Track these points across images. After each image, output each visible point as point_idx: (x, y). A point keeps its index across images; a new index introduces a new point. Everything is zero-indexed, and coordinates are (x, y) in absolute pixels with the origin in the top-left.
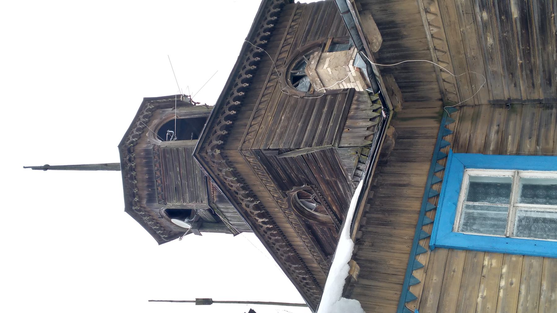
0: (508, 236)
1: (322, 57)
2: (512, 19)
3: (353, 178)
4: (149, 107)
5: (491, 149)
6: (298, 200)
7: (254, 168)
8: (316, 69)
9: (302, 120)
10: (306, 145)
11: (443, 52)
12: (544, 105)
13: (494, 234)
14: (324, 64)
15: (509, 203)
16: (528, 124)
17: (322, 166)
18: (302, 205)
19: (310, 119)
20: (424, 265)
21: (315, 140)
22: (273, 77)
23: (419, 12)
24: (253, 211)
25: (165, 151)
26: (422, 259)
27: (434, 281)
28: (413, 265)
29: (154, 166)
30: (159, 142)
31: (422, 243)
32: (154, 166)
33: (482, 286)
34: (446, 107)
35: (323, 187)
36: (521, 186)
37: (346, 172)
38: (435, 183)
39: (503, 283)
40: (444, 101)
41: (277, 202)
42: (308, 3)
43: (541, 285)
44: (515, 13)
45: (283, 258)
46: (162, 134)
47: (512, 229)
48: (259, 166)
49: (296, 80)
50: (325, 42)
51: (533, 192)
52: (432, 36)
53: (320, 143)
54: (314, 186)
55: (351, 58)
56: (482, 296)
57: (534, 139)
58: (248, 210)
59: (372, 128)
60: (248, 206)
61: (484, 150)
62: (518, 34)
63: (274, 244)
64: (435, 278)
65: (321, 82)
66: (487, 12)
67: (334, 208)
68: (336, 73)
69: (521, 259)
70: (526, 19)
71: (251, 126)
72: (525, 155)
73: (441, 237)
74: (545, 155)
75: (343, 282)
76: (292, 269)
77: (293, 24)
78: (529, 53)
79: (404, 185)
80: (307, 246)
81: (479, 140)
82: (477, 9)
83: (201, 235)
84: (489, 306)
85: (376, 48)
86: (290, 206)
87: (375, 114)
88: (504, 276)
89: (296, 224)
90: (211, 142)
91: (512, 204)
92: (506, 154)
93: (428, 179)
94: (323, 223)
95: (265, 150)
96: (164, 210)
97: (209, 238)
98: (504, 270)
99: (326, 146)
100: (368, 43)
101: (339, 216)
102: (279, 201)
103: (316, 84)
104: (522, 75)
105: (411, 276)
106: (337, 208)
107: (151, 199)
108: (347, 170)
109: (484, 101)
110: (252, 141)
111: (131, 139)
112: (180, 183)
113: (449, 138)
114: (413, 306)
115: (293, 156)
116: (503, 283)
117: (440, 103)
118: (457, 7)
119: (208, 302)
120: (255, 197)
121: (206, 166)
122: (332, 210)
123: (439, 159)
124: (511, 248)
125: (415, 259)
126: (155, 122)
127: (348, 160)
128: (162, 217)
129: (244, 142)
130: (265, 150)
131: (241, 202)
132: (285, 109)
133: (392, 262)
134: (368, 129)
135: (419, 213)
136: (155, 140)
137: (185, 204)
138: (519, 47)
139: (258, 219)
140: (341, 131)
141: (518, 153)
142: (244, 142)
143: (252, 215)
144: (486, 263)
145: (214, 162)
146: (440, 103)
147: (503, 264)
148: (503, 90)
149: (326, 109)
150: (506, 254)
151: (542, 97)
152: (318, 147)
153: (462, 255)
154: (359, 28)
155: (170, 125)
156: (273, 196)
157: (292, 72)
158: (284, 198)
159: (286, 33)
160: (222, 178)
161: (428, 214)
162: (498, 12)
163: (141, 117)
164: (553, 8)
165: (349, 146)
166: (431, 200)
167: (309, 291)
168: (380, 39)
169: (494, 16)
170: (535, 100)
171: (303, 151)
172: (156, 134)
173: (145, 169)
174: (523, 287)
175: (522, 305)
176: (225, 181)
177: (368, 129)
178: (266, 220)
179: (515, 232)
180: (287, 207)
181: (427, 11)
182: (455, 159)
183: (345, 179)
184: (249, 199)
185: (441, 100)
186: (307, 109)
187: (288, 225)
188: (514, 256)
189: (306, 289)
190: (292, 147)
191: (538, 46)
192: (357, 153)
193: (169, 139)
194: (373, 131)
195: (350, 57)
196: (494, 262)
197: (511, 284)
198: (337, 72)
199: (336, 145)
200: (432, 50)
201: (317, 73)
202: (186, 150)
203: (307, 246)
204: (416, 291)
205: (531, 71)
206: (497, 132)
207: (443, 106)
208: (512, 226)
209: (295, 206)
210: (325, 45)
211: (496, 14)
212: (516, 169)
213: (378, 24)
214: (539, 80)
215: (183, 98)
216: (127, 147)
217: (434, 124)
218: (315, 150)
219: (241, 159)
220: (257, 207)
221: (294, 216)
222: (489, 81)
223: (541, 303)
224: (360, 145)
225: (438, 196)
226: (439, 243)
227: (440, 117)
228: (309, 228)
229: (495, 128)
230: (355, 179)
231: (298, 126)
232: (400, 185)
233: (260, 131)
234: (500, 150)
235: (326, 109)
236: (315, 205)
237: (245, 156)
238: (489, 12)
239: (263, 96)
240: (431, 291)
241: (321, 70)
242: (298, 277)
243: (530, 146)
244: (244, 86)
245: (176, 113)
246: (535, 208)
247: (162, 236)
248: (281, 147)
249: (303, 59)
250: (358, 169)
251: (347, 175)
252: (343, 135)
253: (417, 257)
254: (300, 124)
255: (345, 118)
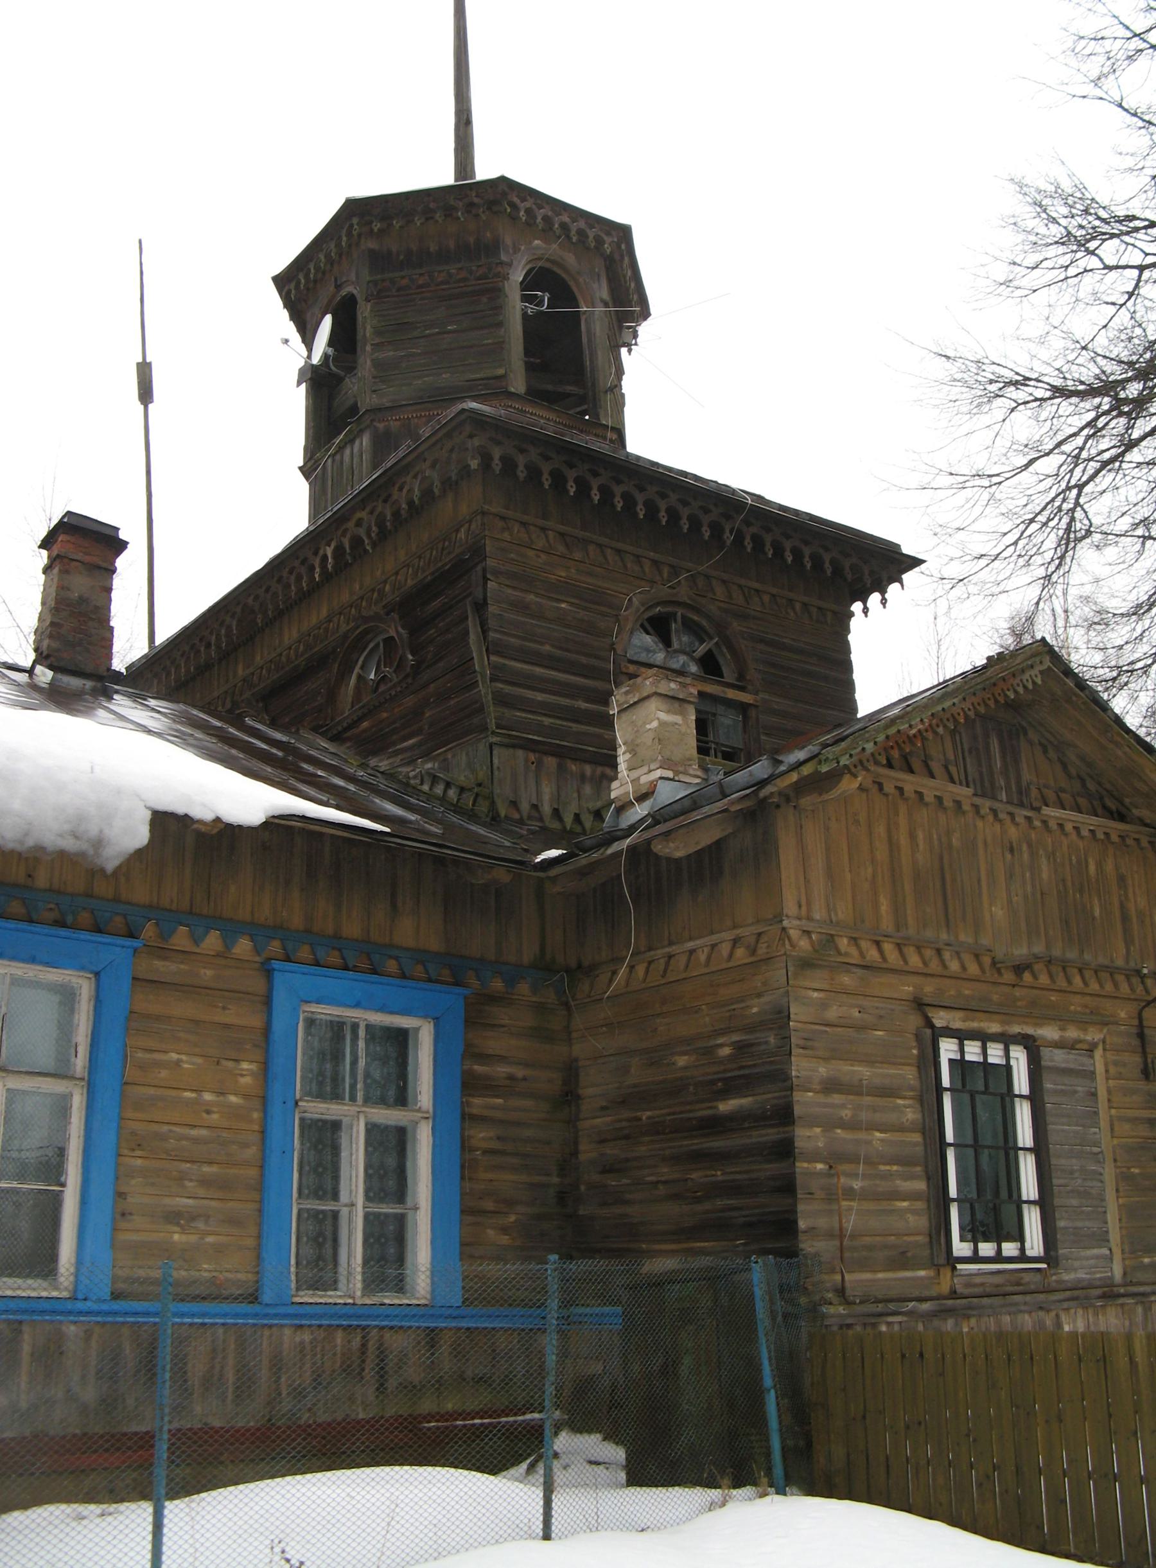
0: (300, 1104)
1: (686, 705)
2: (717, 1100)
3: (428, 773)
4: (608, 240)
5: (476, 1067)
6: (380, 638)
7: (444, 540)
8: (656, 694)
9: (558, 653)
10: (494, 667)
11: (665, 971)
12: (567, 1163)
13: (302, 1078)
14: (668, 712)
15: (367, 1100)
16: (528, 1133)
17: (452, 702)
18: (371, 645)
19: (559, 670)
20: (234, 951)
21: (508, 689)
22: (666, 571)
23: (735, 927)
24: (348, 536)
25: (494, 292)
26: (243, 947)
27: (202, 971)
28: (231, 928)
29: (459, 265)
30: (518, 275)
31: (275, 947)
32: (459, 265)
33: (199, 1060)
34: (565, 976)
35: (410, 701)
36: (401, 1124)
37: (442, 758)
38: (400, 964)
39: (208, 1097)
40: (580, 971)
41: (373, 590)
42: (850, 637)
43: (211, 1163)
44: (726, 1106)
45: (250, 601)
46: (541, 278)
47: (312, 1110)
48: (449, 553)
49: (659, 627)
50: (750, 687)
51: (391, 1147)
52: (692, 952)
53: (502, 700)
54: (410, 680)
55: (676, 773)
56: (182, 1061)
57: (495, 1145)
58: (351, 524)
59: (536, 815)
60: (359, 523)
61: (471, 1053)
62: (690, 1111)
63: (279, 581)
64: (209, 973)
65: (632, 705)
66: (730, 1055)
67: (365, 724)
68: (647, 739)
69: (256, 1127)
70: (716, 1125)
71: (543, 529)
72: (463, 1129)
73: (290, 982)
74: (463, 1167)
75: (181, 809)
76: (228, 619)
77: (798, 606)
78: (658, 1133)
79: (394, 905)
80: (281, 655)
81: (494, 1044)
82: (735, 1038)
83: (299, 384)
84: (164, 1073)
85: (658, 848)
86: (366, 619)
87: (568, 819)
88: (221, 1098)
89: (327, 630)
90: (499, 443)
91: (364, 1109)
92: (463, 1095)
93: (407, 949)
94: (332, 695)
95: (484, 570)
96: (355, 292)
97: (292, 407)
98: (233, 1099)
99: (492, 712)
100: (667, 834)
101: (348, 734)
102: (375, 595)
103: (627, 693)
104: (620, 1121)
105: (208, 929)
106: (364, 731)
107: (379, 261)
108: (445, 760)
109: (577, 1049)
110: (506, 536)
111: (522, 206)
112: (416, 333)
113: (498, 985)
114: (151, 934)
115: (472, 637)
116: (208, 1097)
117: (573, 964)
118: (741, 999)
119: (146, 394)
120: (384, 535)
121: (440, 434)
122: (360, 719)
123: (446, 968)
124: (276, 1110)
125: (244, 934)
126: (570, 259)
127: (464, 764)
128: (338, 287)
129: (503, 518)
130: (484, 570)
131: (368, 509)
132: (585, 609)
133: (233, 889)
134: (535, 807)
135: (337, 936)
136: (523, 262)
137: (368, 348)
138: (669, 1114)
139: (332, 546)
140: (529, 746)
141: (468, 1118)
142: (503, 518)
143: (340, 532)
144: (245, 1066)
145: (452, 450)
146: (573, 964)
147: (245, 1096)
148: (595, 1086)
149: (584, 705)
150: (264, 1101)
151: (582, 1157)
152: (490, 697)
153: (256, 1021)
154: (696, 816)
155: (563, 293)
156: (385, 582)
157: (679, 614)
158: (384, 607)
159: (774, 591)
160: (417, 469)
161: (337, 953)
162: (729, 1075)
163: (582, 224)
164: (732, 1173)
165: (495, 766)
166: (365, 960)
167: (182, 655)
168: (679, 854)
169: (722, 1068)
170: (576, 1143)
171: (481, 662)
172: (540, 264)
173: (452, 244)
174: (204, 1132)
175: (170, 1131)
176: (412, 474)
177: (535, 807)
178: (329, 566)
179: (307, 1115)
180: (364, 613)
181: (735, 942)
182: (452, 1000)
183: (426, 755)
184: (374, 528)
185: (580, 966)
186: (584, 660)
187: (324, 612)
188: (262, 1115)
189: (187, 648)
190: (492, 635)
191: (670, 1148)
192: (480, 785)
193: (525, 299)
194: (530, 818)
195: (681, 769)
196: (247, 1080)
197: (208, 1112)
198: (649, 743)
199: (494, 739)
200: (667, 950)
201: (648, 697)
202: (498, 349)
203: (281, 655)
204: (181, 938)
205: (627, 1137)
206: (511, 1078)
207: (568, 971)
208: (318, 1110)
209: (366, 632)
210: (742, 689)
211: (725, 1071)
212: (434, 1112)
213: (718, 845)
214: (612, 1151)
215: (630, 327)
216: (505, 191)
217: (529, 954)
218: (484, 690)
219: (464, 510)
220: (357, 542)
221: (344, 628)
222: (612, 1058)
223: (176, 1163)
224: (497, 791)
225: (374, 972)
226: (278, 978)
227: (544, 967)
228: (319, 663)
229: (519, 1072)
230: (426, 778)
231: (542, 644)
232: (394, 896)
233: (531, 553)
234: (471, 1085)
235: (584, 705)
236: (372, 676)
237: (470, 522)
238: (731, 1058)
239: (619, 551)
240: (182, 966)
241: (653, 705)
242: (211, 633)
243: (483, 1139)
244: (638, 508)
245: (594, 309)
246: (357, 1150)
247: (292, 286)
248: (492, 609)
249: (711, 638)
250: (448, 785)
251: (434, 759)
252: (520, 753)
253: (248, 937)
254: (547, 648)
255: (560, 753)
